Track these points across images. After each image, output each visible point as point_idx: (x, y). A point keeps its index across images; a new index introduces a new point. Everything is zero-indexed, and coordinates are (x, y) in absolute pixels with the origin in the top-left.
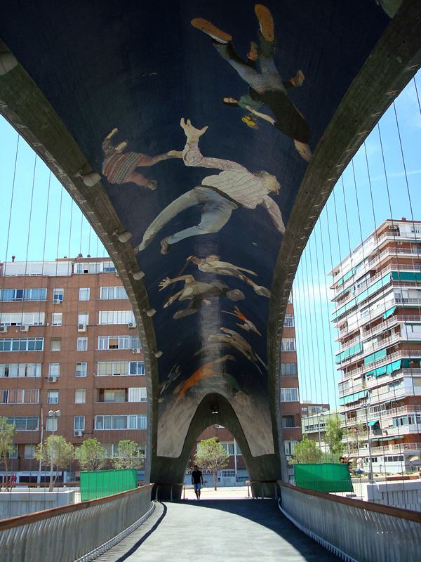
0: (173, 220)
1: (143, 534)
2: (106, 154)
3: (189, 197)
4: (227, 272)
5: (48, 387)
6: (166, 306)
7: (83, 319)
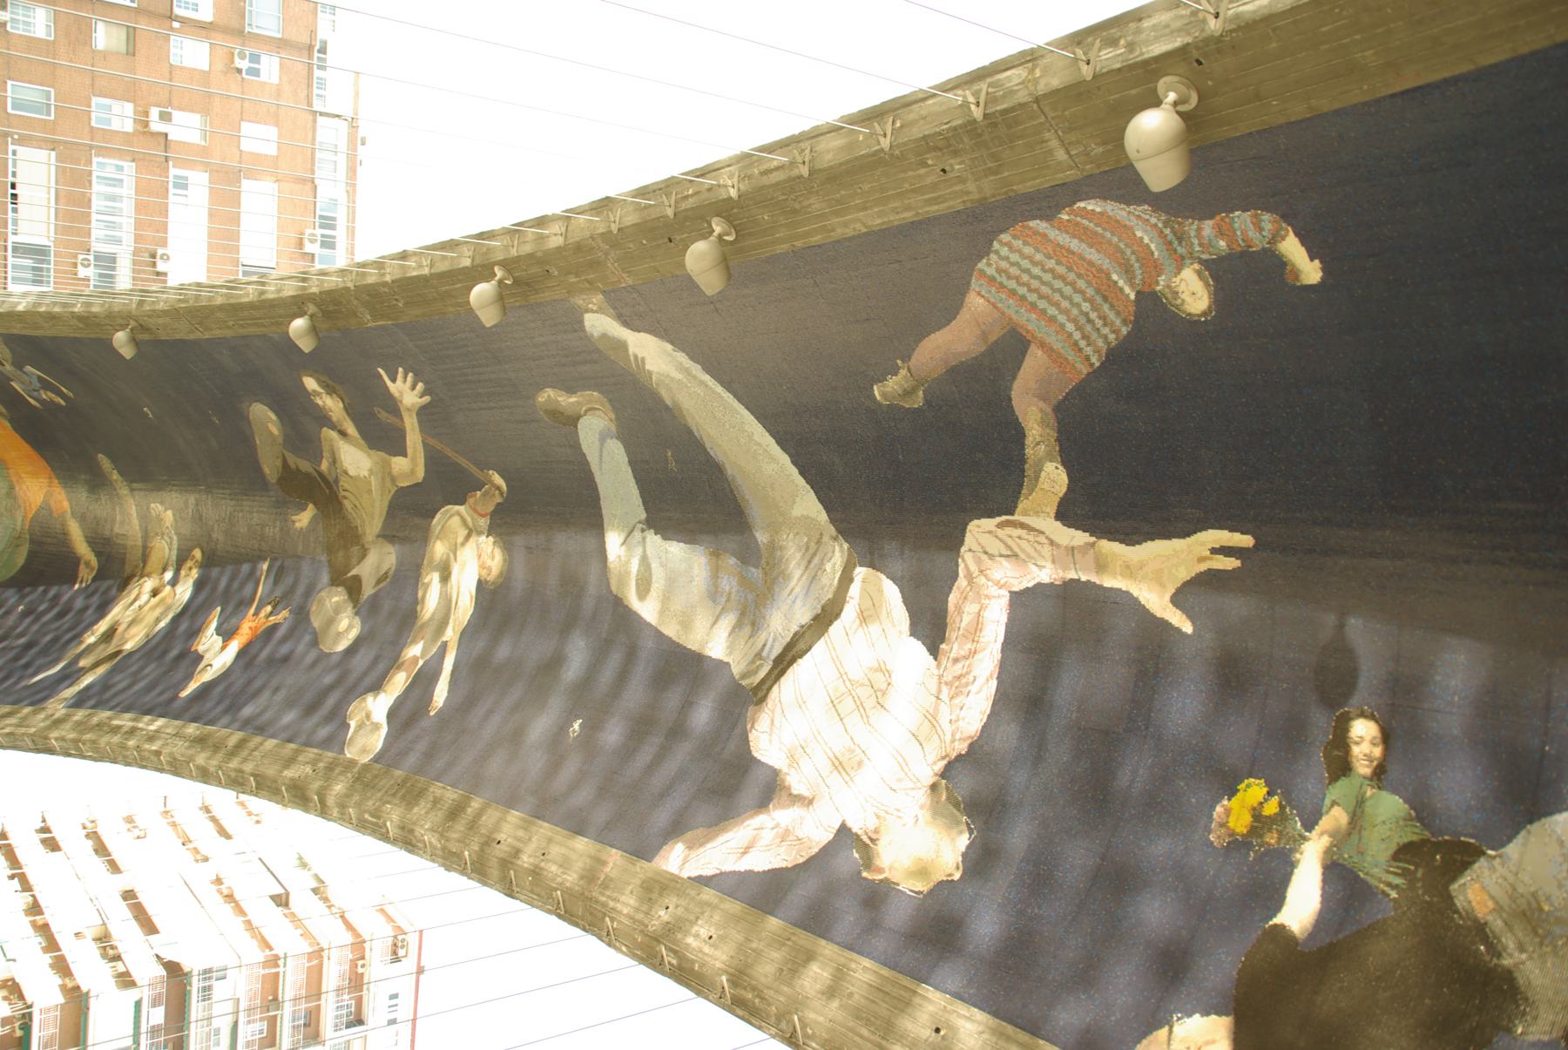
3: (797, 511)
6: (311, 383)
7: (185, 127)
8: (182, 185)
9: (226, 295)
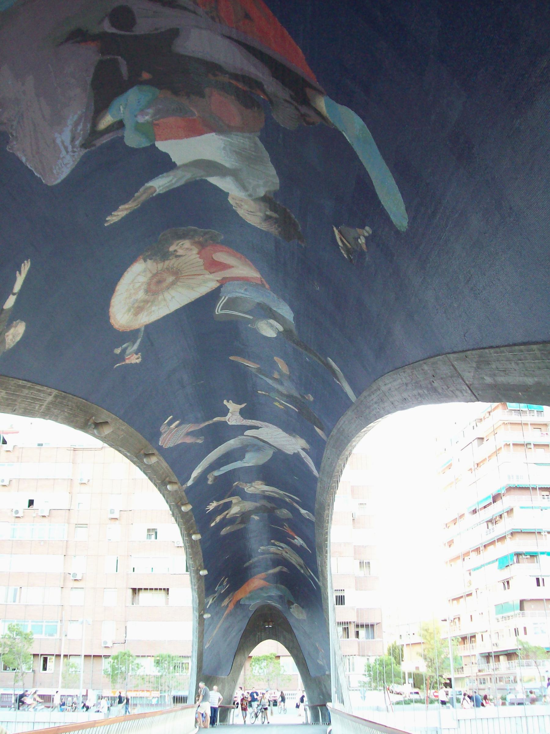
0: (219, 459)
2: (163, 431)
4: (275, 494)
6: (213, 524)
9: (189, 549)
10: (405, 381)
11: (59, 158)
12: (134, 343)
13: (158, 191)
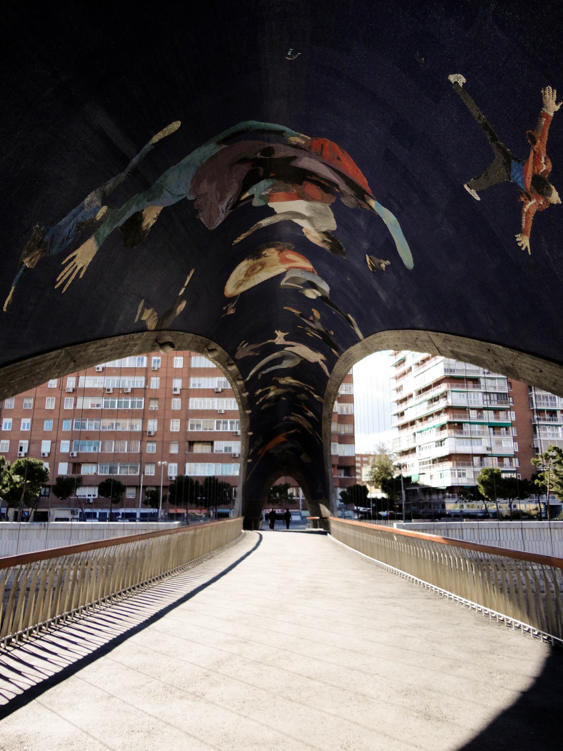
1: (82, 652)
5: (147, 439)
6: (257, 403)
7: (177, 384)
8: (194, 385)
10: (398, 336)
11: (218, 216)
12: (233, 303)
13: (263, 225)
